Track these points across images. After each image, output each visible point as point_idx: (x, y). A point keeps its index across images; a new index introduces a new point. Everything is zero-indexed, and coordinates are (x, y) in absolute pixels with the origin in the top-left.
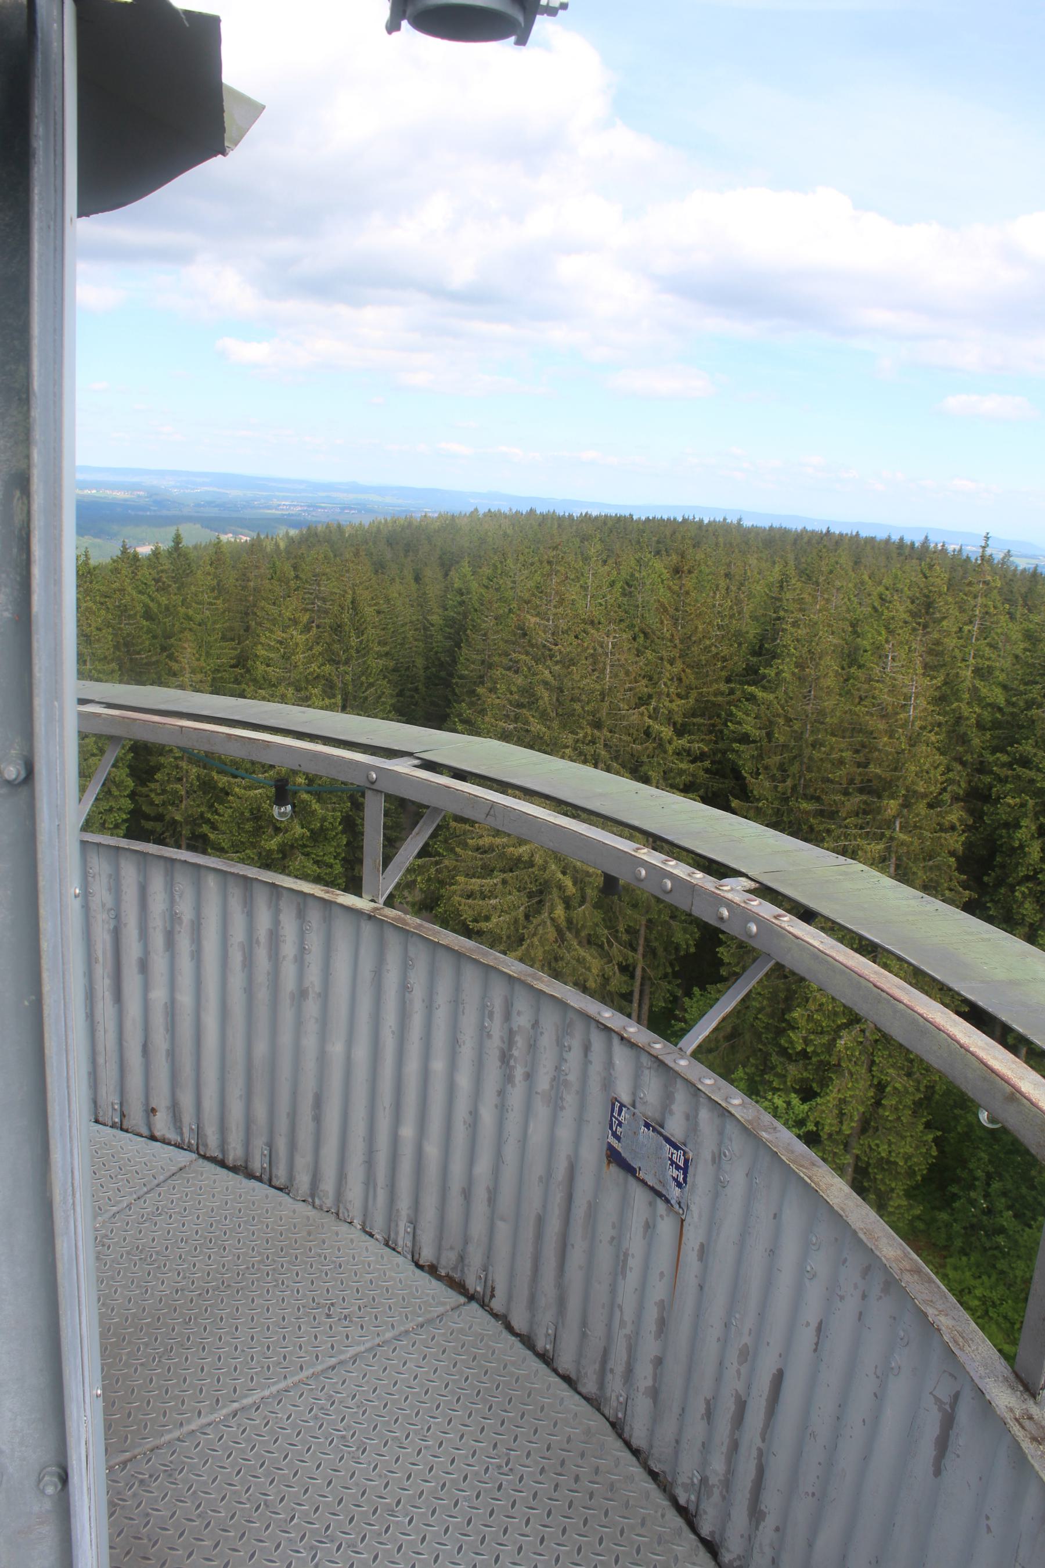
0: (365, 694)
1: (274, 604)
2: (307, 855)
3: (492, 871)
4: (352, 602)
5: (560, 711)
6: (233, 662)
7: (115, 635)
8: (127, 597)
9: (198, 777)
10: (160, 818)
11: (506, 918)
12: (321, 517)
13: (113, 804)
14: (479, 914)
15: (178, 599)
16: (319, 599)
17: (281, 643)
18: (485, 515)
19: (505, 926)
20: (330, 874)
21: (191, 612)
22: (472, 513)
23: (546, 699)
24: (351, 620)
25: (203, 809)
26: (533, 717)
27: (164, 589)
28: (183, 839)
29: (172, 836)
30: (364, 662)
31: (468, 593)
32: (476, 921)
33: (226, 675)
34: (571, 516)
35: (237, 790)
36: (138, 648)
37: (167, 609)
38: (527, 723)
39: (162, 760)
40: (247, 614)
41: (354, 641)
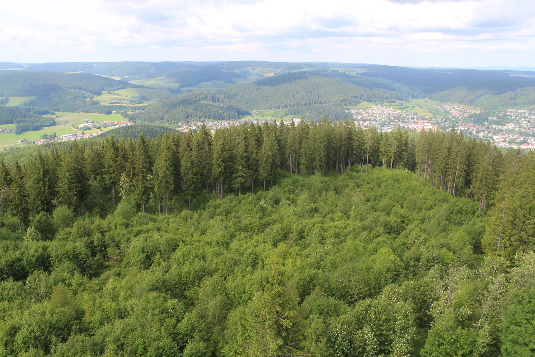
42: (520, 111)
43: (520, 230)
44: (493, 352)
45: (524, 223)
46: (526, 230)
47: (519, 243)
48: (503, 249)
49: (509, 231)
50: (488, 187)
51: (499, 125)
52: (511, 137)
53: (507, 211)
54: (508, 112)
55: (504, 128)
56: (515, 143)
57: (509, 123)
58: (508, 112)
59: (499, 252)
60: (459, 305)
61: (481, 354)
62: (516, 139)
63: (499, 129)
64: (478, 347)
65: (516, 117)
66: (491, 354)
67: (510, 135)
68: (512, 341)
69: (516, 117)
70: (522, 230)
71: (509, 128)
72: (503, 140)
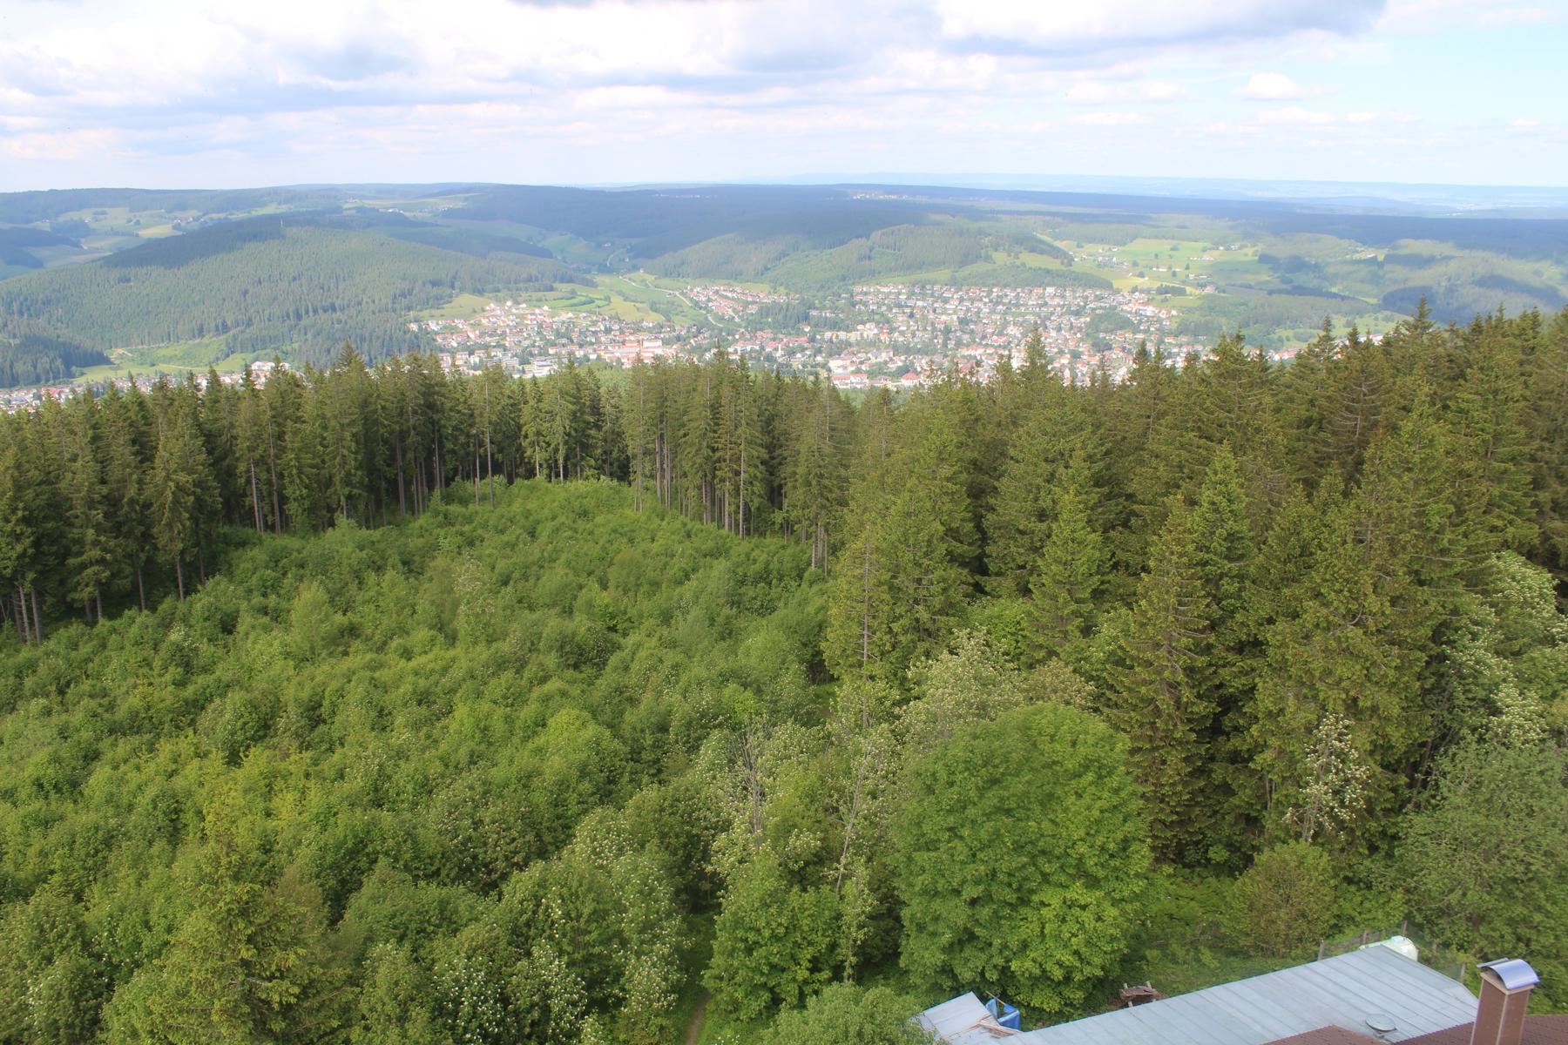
42: (886, 290)
44: (887, 932)
45: (919, 581)
49: (886, 608)
52: (873, 360)
53: (874, 556)
55: (853, 337)
57: (864, 323)
59: (870, 667)
62: (886, 363)
66: (882, 940)
68: (925, 892)
70: (917, 602)
72: (853, 368)
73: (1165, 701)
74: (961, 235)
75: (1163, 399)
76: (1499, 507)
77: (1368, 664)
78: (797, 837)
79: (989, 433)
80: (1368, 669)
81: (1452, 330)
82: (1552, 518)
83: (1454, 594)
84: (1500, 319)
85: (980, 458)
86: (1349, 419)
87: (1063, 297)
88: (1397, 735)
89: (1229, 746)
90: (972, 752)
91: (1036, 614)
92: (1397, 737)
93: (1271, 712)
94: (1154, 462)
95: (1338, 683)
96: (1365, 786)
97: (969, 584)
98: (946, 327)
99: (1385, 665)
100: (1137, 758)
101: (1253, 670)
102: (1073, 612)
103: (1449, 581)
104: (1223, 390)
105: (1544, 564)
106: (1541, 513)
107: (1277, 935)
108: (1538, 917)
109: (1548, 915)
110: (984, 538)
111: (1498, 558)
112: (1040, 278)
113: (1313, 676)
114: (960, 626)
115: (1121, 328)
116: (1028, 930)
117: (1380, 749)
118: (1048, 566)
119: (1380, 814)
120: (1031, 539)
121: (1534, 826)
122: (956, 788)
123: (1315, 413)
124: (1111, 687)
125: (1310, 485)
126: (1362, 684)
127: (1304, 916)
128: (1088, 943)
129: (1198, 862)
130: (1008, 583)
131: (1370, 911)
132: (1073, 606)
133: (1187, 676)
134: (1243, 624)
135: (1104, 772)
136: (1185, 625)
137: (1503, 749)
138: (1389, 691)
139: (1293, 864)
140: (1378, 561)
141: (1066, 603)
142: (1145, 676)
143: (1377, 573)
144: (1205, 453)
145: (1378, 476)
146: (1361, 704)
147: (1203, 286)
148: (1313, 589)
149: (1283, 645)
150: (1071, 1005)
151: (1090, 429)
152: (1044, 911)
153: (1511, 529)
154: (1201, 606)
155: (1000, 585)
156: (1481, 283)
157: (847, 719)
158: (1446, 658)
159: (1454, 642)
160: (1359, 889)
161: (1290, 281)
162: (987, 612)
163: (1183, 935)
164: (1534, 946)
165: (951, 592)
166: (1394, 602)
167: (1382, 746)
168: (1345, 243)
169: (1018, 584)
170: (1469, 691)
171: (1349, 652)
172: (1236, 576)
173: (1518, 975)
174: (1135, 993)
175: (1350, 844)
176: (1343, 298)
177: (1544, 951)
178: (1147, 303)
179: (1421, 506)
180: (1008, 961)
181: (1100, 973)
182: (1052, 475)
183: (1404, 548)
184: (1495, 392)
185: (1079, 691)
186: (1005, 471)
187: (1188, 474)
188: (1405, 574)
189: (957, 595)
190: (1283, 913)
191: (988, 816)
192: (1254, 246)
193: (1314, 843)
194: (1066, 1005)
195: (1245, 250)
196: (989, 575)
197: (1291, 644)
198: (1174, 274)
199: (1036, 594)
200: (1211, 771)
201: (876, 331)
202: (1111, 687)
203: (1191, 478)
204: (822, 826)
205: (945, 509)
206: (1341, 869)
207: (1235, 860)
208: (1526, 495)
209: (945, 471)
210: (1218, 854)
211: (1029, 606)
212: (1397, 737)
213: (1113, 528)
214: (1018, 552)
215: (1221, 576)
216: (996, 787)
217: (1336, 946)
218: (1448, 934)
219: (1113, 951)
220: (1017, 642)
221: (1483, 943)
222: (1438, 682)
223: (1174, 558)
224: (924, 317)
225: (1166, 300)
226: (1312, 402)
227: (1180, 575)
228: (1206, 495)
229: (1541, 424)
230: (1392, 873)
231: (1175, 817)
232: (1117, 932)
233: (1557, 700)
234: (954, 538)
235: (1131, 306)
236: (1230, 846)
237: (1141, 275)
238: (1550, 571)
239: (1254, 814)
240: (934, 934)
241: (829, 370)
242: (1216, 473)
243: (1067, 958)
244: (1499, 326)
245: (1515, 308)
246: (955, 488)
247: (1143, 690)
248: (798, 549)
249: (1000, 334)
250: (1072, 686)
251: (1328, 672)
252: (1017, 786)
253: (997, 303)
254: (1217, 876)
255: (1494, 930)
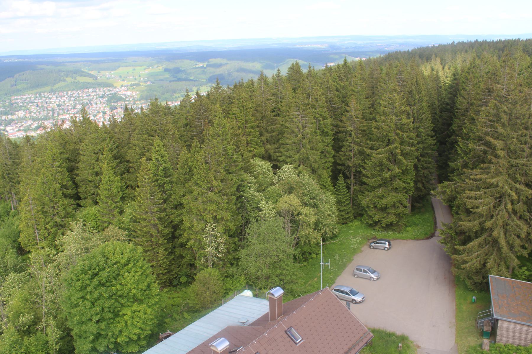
0: (421, 117)
1: (385, 83)
2: (400, 179)
3: (480, 188)
4: (416, 82)
5: (510, 123)
6: (370, 106)
7: (326, 98)
8: (330, 84)
9: (358, 150)
10: (343, 165)
11: (486, 207)
12: (393, 49)
13: (326, 160)
14: (474, 206)
15: (347, 83)
16: (401, 81)
17: (390, 99)
18: (457, 43)
19: (485, 211)
20: (409, 186)
21: (353, 88)
22: (452, 43)
23: (505, 118)
24: (416, 88)
25: (360, 161)
26: (500, 126)
27: (341, 80)
28: (352, 172)
29: (348, 171)
30: (421, 105)
31: (458, 75)
32: (472, 208)
33: (367, 111)
34: (493, 41)
35: (374, 155)
36: (334, 102)
37: (344, 87)
38: (497, 128)
39: (344, 143)
40: (373, 88)
41: (417, 97)
42: (25, 97)
43: (52, 216)
44: (69, 342)
45: (54, 207)
46: (58, 214)
47: (56, 229)
48: (44, 240)
49: (43, 220)
50: (13, 182)
51: (8, 115)
52: (25, 125)
53: (34, 201)
54: (13, 100)
55: (15, 117)
56: (31, 130)
57: (18, 111)
58: (13, 100)
59: (41, 244)
60: (18, 315)
61: (58, 351)
62: (30, 125)
63: (10, 119)
64: (52, 347)
65: (23, 103)
66: (67, 346)
67: (23, 123)
68: (79, 323)
69: (23, 103)
70: (54, 215)
71: (20, 116)
72: (17, 129)
73: (153, 231)
74: (52, 73)
75: (134, 125)
76: (251, 144)
77: (217, 204)
78: (23, 317)
79: (71, 147)
80: (218, 205)
81: (228, 88)
82: (267, 145)
83: (241, 175)
84: (243, 82)
85: (70, 157)
86: (199, 122)
87: (96, 92)
88: (231, 225)
89: (179, 242)
90: (83, 266)
91: (101, 210)
92: (232, 226)
93: (189, 227)
94: (134, 148)
95: (209, 212)
96: (225, 244)
97: (74, 204)
98: (52, 109)
99: (223, 203)
100: (148, 253)
101: (182, 214)
102: (115, 207)
103: (239, 171)
104: (154, 119)
105: (267, 160)
106: (264, 144)
107: (208, 301)
108: (284, 272)
109: (287, 270)
110: (77, 186)
111: (253, 160)
112: (85, 86)
113: (201, 212)
114: (73, 221)
115: (119, 101)
116: (120, 326)
117: (227, 231)
118: (102, 192)
119: (232, 252)
120: (94, 183)
121: (278, 244)
122: (81, 281)
123: (188, 122)
124: (134, 231)
125: (189, 147)
126: (217, 211)
127: (215, 292)
128: (144, 323)
129: (178, 284)
130: (89, 201)
131: (235, 285)
132: (114, 205)
133: (160, 221)
134: (175, 199)
135: (135, 262)
136: (155, 203)
137: (264, 222)
138: (226, 211)
139: (207, 276)
140: (214, 169)
141: (112, 204)
142: (145, 224)
143: (215, 173)
144: (151, 141)
145: (209, 140)
146: (218, 217)
147: (146, 82)
148: (195, 182)
149: (189, 203)
150: (143, 347)
151: (109, 139)
152: (125, 317)
153: (256, 150)
154: (159, 195)
155: (86, 202)
156: (238, 71)
157: (36, 266)
158: (243, 196)
159: (244, 190)
160: (231, 279)
161: (176, 77)
162: (83, 213)
163: (177, 311)
164: (285, 281)
165: (68, 209)
166: (222, 181)
167: (228, 230)
168: (192, 62)
169: (93, 201)
170: (252, 205)
171: (210, 201)
172: (169, 183)
173: (278, 292)
174: (165, 336)
175: (225, 264)
176: (195, 81)
177: (288, 282)
178: (127, 90)
179: (225, 148)
180: (116, 339)
181: (150, 332)
182: (98, 158)
183: (222, 163)
184: (243, 107)
185: (122, 235)
186: (80, 160)
187: (146, 150)
188: (223, 171)
189: (70, 209)
190: (208, 293)
191: (95, 288)
192: (162, 66)
193: (213, 267)
194: (141, 347)
195: (159, 68)
196: (82, 200)
197: (191, 202)
198: (135, 79)
199: (100, 203)
200: (175, 252)
201: (24, 114)
202: (134, 231)
203: (148, 151)
204: (33, 310)
205: (59, 178)
206: (224, 273)
207: (190, 280)
208: (258, 139)
209: (57, 164)
210: (183, 279)
211: (98, 208)
212: (232, 226)
213: (124, 173)
214: (91, 189)
215: (164, 183)
216: (96, 277)
217: (227, 299)
218: (260, 285)
219: (153, 324)
220: (97, 222)
221: (270, 285)
222: (242, 205)
223: (146, 180)
224: (43, 106)
225: (134, 88)
226: (186, 118)
227: (150, 186)
228: (153, 156)
229: (259, 115)
230: (240, 270)
231: (166, 271)
232: (151, 317)
233: (278, 202)
234: (65, 188)
235: (122, 92)
236: (187, 276)
237: (124, 81)
238: (269, 162)
239: (192, 263)
240: (86, 338)
241: (7, 131)
242: (155, 148)
243: (137, 331)
244: (241, 85)
245: (246, 78)
246: (61, 170)
247: (145, 229)
248: (5, 204)
249: (74, 108)
250: (119, 233)
251: (205, 209)
252: (104, 274)
253: (71, 97)
254: (185, 287)
255: (273, 279)
